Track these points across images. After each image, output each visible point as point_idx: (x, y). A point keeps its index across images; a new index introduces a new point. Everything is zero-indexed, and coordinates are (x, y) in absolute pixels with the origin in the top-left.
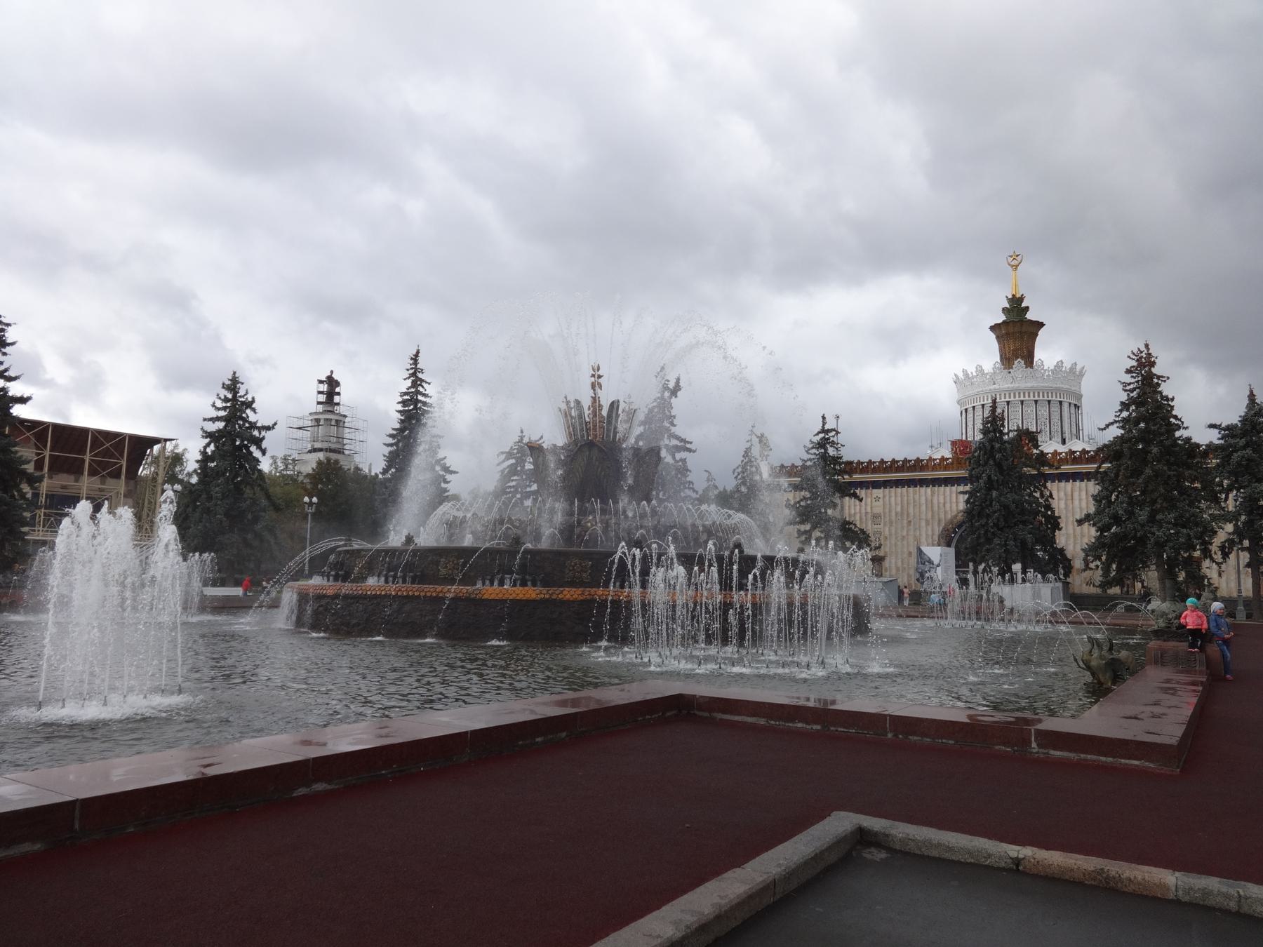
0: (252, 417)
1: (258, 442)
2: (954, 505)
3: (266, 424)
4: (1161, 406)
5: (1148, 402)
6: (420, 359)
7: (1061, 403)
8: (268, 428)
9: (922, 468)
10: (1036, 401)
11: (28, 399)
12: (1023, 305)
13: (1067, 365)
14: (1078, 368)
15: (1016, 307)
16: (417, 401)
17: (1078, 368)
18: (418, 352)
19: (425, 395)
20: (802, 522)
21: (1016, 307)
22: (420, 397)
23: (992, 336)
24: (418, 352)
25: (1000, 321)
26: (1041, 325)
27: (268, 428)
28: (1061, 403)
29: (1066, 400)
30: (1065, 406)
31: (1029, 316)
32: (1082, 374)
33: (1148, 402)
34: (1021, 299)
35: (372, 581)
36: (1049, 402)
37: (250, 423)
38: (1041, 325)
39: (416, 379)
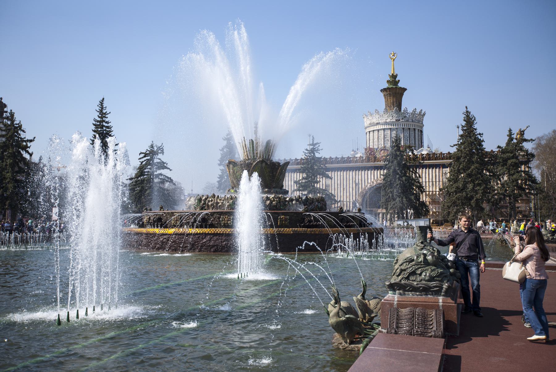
0: (23, 135)
1: (25, 148)
2: (342, 174)
3: (29, 139)
4: (476, 139)
5: (470, 135)
6: (104, 102)
7: (414, 129)
8: (31, 141)
9: (350, 162)
10: (403, 129)
11: (41, 156)
12: (397, 79)
13: (418, 111)
14: (423, 112)
15: (394, 79)
16: (103, 126)
17: (423, 112)
18: (103, 99)
19: (107, 123)
20: (304, 190)
21: (394, 79)
22: (104, 124)
23: (382, 94)
24: (103, 99)
25: (386, 87)
26: (405, 90)
27: (31, 141)
28: (414, 129)
29: (417, 128)
30: (417, 131)
31: (400, 85)
32: (424, 115)
33: (470, 135)
34: (396, 76)
35: (444, 286)
36: (409, 129)
37: (21, 138)
38: (405, 90)
39: (103, 114)
